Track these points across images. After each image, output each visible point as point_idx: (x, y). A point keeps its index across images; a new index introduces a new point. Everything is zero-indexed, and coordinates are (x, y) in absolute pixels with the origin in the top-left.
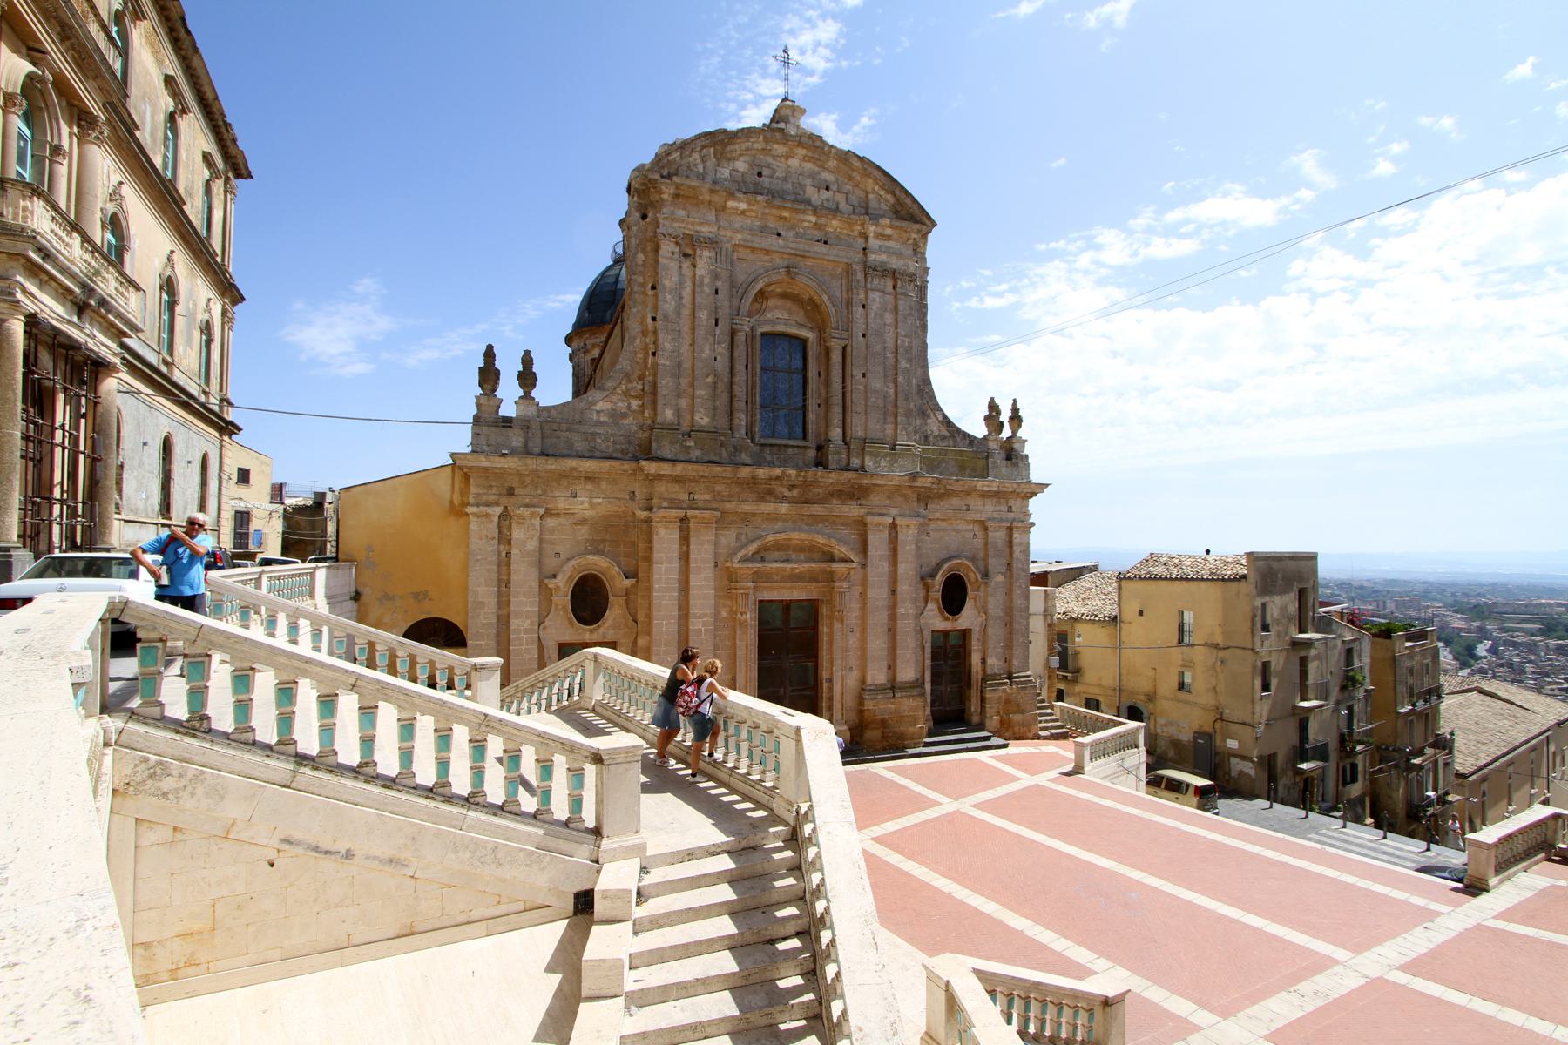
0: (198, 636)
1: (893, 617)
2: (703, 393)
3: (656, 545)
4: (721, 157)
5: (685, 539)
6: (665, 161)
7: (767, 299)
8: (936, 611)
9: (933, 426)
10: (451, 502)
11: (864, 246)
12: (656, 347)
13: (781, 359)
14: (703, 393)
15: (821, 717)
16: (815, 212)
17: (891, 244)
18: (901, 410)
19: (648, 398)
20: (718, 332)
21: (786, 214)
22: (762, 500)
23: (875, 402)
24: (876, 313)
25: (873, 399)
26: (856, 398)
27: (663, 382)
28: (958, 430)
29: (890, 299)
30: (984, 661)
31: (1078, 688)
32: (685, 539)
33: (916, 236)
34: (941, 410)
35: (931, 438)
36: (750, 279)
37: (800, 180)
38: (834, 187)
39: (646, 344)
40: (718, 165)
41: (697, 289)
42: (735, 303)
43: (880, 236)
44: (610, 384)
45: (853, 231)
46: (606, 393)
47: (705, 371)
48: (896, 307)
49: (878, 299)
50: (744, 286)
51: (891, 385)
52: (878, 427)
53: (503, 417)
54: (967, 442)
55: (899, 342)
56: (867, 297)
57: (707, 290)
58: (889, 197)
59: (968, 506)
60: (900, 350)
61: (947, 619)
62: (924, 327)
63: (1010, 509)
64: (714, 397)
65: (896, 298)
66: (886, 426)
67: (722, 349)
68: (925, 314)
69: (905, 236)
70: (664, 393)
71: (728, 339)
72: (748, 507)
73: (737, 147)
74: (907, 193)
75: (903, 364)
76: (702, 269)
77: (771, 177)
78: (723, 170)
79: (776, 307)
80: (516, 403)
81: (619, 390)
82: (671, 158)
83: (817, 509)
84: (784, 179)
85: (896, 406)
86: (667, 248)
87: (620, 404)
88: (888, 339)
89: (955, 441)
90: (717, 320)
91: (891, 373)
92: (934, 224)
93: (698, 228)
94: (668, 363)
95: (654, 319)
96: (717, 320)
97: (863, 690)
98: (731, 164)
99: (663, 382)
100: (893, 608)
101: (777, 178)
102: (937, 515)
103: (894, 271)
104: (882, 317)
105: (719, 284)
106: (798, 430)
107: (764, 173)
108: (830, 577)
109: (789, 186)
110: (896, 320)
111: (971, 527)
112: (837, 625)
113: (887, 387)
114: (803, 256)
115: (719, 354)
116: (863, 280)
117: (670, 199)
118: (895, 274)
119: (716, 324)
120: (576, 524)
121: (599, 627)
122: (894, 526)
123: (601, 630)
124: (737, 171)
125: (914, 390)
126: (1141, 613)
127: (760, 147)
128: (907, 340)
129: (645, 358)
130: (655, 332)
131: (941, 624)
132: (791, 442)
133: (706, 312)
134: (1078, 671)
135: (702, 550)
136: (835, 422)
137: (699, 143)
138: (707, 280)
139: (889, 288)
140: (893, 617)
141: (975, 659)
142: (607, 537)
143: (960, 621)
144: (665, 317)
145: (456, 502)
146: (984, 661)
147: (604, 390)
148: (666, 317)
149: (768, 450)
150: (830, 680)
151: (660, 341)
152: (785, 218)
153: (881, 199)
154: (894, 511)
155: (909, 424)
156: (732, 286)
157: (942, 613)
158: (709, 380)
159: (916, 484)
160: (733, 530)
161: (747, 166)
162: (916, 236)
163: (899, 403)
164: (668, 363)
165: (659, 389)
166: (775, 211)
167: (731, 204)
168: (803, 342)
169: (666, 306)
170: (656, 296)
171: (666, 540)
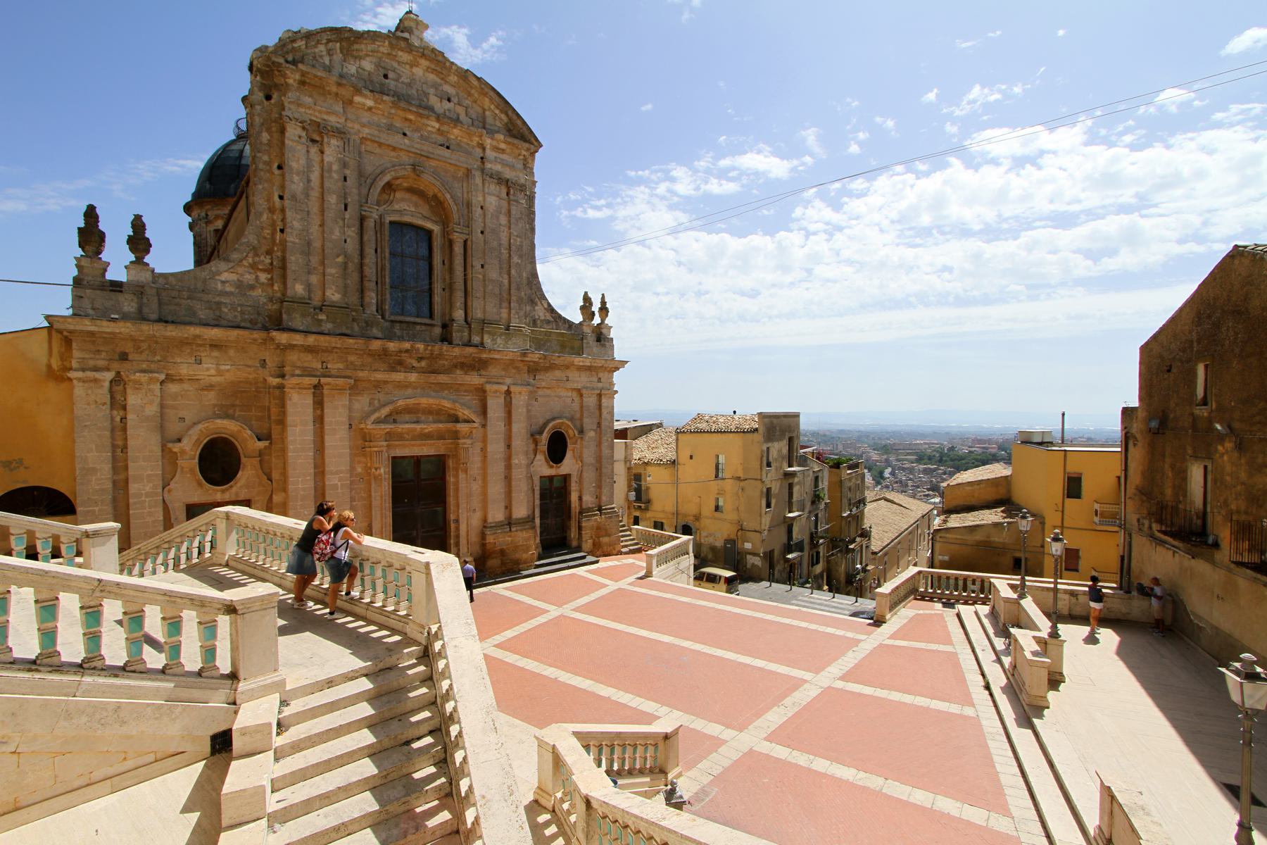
1: (509, 467)
2: (333, 271)
3: (290, 409)
4: (348, 53)
5: (319, 403)
9: (540, 312)
12: (285, 224)
14: (333, 271)
15: (450, 552)
16: (438, 119)
17: (504, 157)
18: (514, 298)
20: (347, 216)
21: (412, 117)
22: (392, 369)
25: (490, 287)
27: (293, 258)
28: (560, 316)
29: (505, 204)
30: (580, 498)
31: (649, 514)
33: (525, 153)
35: (539, 322)
36: (378, 171)
38: (455, 100)
41: (326, 175)
43: (496, 149)
45: (472, 141)
46: (232, 264)
48: (509, 211)
51: (506, 276)
54: (567, 326)
55: (512, 241)
56: (484, 200)
57: (335, 176)
58: (503, 116)
60: (513, 248)
61: (552, 467)
62: (533, 230)
63: (599, 380)
66: (502, 310)
67: (352, 233)
68: (533, 220)
69: (517, 152)
70: (293, 268)
71: (357, 223)
72: (380, 376)
73: (364, 47)
74: (518, 115)
75: (515, 259)
78: (350, 66)
79: (403, 200)
81: (245, 263)
83: (443, 378)
85: (510, 294)
86: (293, 131)
93: (325, 117)
94: (297, 241)
95: (281, 197)
97: (485, 527)
99: (293, 258)
100: (509, 459)
101: (402, 83)
102: (544, 384)
104: (498, 218)
105: (347, 172)
106: (426, 310)
108: (456, 435)
111: (570, 394)
114: (427, 157)
117: (295, 85)
118: (507, 183)
119: (346, 209)
120: (202, 389)
122: (508, 392)
124: (364, 70)
126: (691, 457)
127: (386, 52)
130: (283, 210)
131: (547, 471)
133: (335, 196)
134: (649, 502)
135: (337, 413)
137: (325, 37)
138: (335, 167)
139: (504, 195)
140: (509, 467)
141: (574, 497)
142: (238, 402)
143: (562, 468)
146: (580, 498)
148: (294, 197)
149: (397, 326)
150: (457, 521)
151: (289, 220)
152: (410, 121)
153: (496, 118)
154: (508, 381)
156: (361, 174)
157: (547, 462)
158: (340, 259)
159: (527, 359)
161: (373, 66)
162: (525, 153)
163: (512, 292)
164: (297, 241)
166: (401, 113)
167: (357, 99)
168: (429, 233)
169: (294, 187)
170: (283, 176)
171: (299, 406)
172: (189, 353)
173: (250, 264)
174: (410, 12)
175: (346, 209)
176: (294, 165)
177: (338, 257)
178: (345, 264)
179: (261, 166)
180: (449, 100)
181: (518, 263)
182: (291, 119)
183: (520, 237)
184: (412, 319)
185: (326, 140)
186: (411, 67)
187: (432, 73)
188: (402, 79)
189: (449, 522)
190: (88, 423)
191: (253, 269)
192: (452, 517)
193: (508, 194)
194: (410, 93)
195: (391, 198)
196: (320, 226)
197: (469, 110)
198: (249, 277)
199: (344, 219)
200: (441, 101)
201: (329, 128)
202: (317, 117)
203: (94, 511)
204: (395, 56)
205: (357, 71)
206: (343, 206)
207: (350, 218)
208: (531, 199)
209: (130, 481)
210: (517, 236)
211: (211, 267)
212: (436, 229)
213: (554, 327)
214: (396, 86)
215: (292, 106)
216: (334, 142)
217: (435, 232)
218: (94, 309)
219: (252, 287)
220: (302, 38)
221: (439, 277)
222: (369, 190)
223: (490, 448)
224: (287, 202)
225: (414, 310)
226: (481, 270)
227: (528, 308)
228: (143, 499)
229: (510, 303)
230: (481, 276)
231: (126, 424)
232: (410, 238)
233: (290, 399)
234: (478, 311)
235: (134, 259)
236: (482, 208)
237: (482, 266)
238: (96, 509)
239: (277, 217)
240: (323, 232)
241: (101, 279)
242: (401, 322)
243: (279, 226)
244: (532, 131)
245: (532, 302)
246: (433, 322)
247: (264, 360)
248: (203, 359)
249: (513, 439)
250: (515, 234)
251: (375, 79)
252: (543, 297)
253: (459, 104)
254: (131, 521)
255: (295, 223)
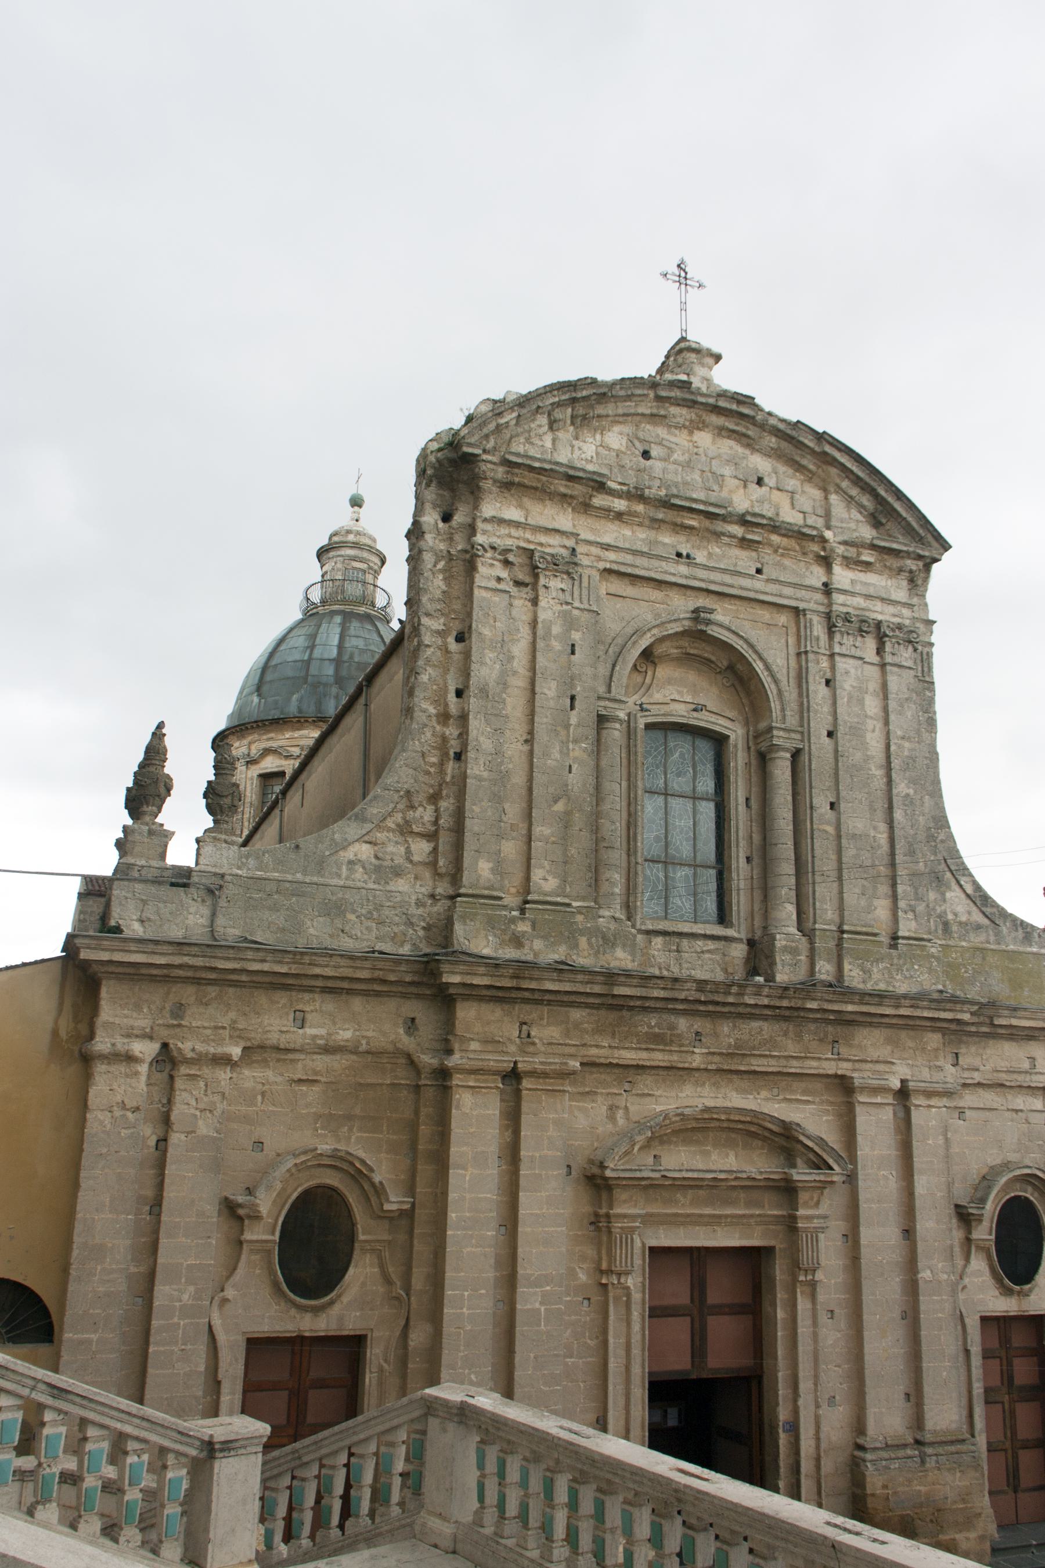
0: (666, 898)
1: (912, 1287)
2: (547, 831)
3: (457, 1128)
5: (513, 1118)
6: (492, 426)
7: (655, 664)
8: (987, 1277)
9: (956, 904)
10: (55, 1033)
11: (824, 579)
12: (465, 745)
13: (679, 775)
14: (547, 831)
15: (776, 1490)
18: (901, 871)
19: (445, 839)
20: (574, 720)
23: (856, 856)
24: (850, 697)
25: (852, 852)
26: (823, 853)
27: (476, 809)
28: (1004, 914)
29: (874, 672)
32: (513, 1118)
34: (971, 875)
35: (955, 928)
36: (629, 630)
37: (714, 469)
38: (770, 481)
39: (444, 739)
40: (577, 439)
41: (540, 644)
42: (603, 670)
44: (374, 810)
46: (368, 826)
47: (551, 790)
48: (884, 686)
49: (853, 671)
50: (620, 641)
51: (883, 827)
52: (863, 903)
53: (174, 867)
54: (1020, 934)
55: (893, 748)
56: (833, 667)
57: (556, 645)
59: (1032, 1059)
60: (896, 763)
62: (931, 723)
64: (564, 839)
65: (884, 673)
66: (876, 902)
67: (580, 751)
68: (931, 701)
70: (476, 829)
71: (592, 733)
74: (899, 495)
75: (901, 788)
76: (549, 608)
77: (665, 460)
78: (585, 447)
79: (669, 681)
80: (198, 841)
81: (390, 823)
82: (502, 421)
84: (688, 465)
85: (893, 865)
86: (488, 571)
87: (391, 848)
88: (874, 743)
89: (998, 934)
90: (573, 698)
91: (881, 805)
92: (946, 546)
94: (485, 774)
95: (459, 693)
96: (573, 698)
97: (860, 1447)
98: (598, 437)
99: (476, 809)
100: (911, 1264)
101: (675, 463)
103: (879, 624)
104: (861, 702)
105: (576, 636)
106: (710, 904)
107: (654, 453)
108: (788, 1190)
109: (696, 476)
110: (886, 710)
112: (803, 1304)
113: (875, 828)
115: (575, 759)
116: (824, 638)
118: (880, 634)
119: (572, 708)
121: (332, 1303)
123: (336, 1310)
124: (609, 449)
125: (922, 836)
128: (907, 745)
129: (442, 764)
130: (463, 718)
132: (699, 929)
133: (553, 685)
136: (784, 891)
138: (556, 630)
139: (871, 655)
140: (912, 1287)
142: (357, 1111)
144: (481, 690)
145: (63, 1034)
147: (364, 820)
148: (484, 692)
149: (658, 941)
150: (794, 1428)
151: (473, 733)
155: (919, 898)
156: (598, 639)
157: (999, 1280)
158: (560, 807)
160: (600, 1099)
161: (624, 441)
163: (899, 858)
164: (485, 774)
165: (468, 823)
168: (719, 741)
169: (484, 671)
170: (467, 655)
172: (284, 1005)
173: (398, 825)
174: (262, 1150)
175: (572, 708)
176: (486, 632)
177: (556, 802)
178: (568, 813)
179: (427, 639)
180: (760, 482)
181: (908, 795)
182: (485, 550)
183: (909, 739)
184: (686, 928)
185: (542, 581)
186: (691, 433)
187: (729, 437)
188: (675, 456)
189: (774, 1428)
190: (104, 1150)
191: (402, 834)
192: (783, 1414)
193: (880, 651)
194: (689, 479)
195: (648, 680)
196: (526, 741)
197: (797, 496)
198: (394, 850)
199: (567, 727)
200: (745, 487)
201: (549, 558)
202: (529, 542)
203: (89, 1342)
204: (665, 417)
205: (597, 454)
206: (568, 701)
207: (578, 725)
208: (925, 661)
209: (159, 1277)
210: (903, 738)
211: (334, 833)
212: (736, 733)
213: (992, 938)
214: (664, 470)
215: (488, 527)
216: (556, 584)
217: (733, 737)
218: (142, 921)
219: (397, 872)
220: (512, 409)
221: (741, 834)
222: (614, 666)
223: (866, 1235)
224: (474, 703)
225: (688, 905)
226: (830, 815)
227: (932, 895)
228: (176, 1320)
229: (894, 885)
230: (830, 829)
231: (165, 1151)
232: (682, 755)
233: (458, 1107)
234: (827, 906)
235: (211, 825)
236: (828, 682)
237: (832, 805)
238: (94, 1337)
239: (452, 731)
240: (531, 753)
241: (159, 864)
242: (664, 933)
243: (454, 746)
244: (927, 522)
245: (938, 880)
246: (730, 932)
247: (413, 1020)
248: (309, 1017)
249: (918, 1216)
250: (899, 733)
251: (626, 461)
252: (958, 870)
253: (779, 489)
254: (150, 1370)
255: (482, 739)
